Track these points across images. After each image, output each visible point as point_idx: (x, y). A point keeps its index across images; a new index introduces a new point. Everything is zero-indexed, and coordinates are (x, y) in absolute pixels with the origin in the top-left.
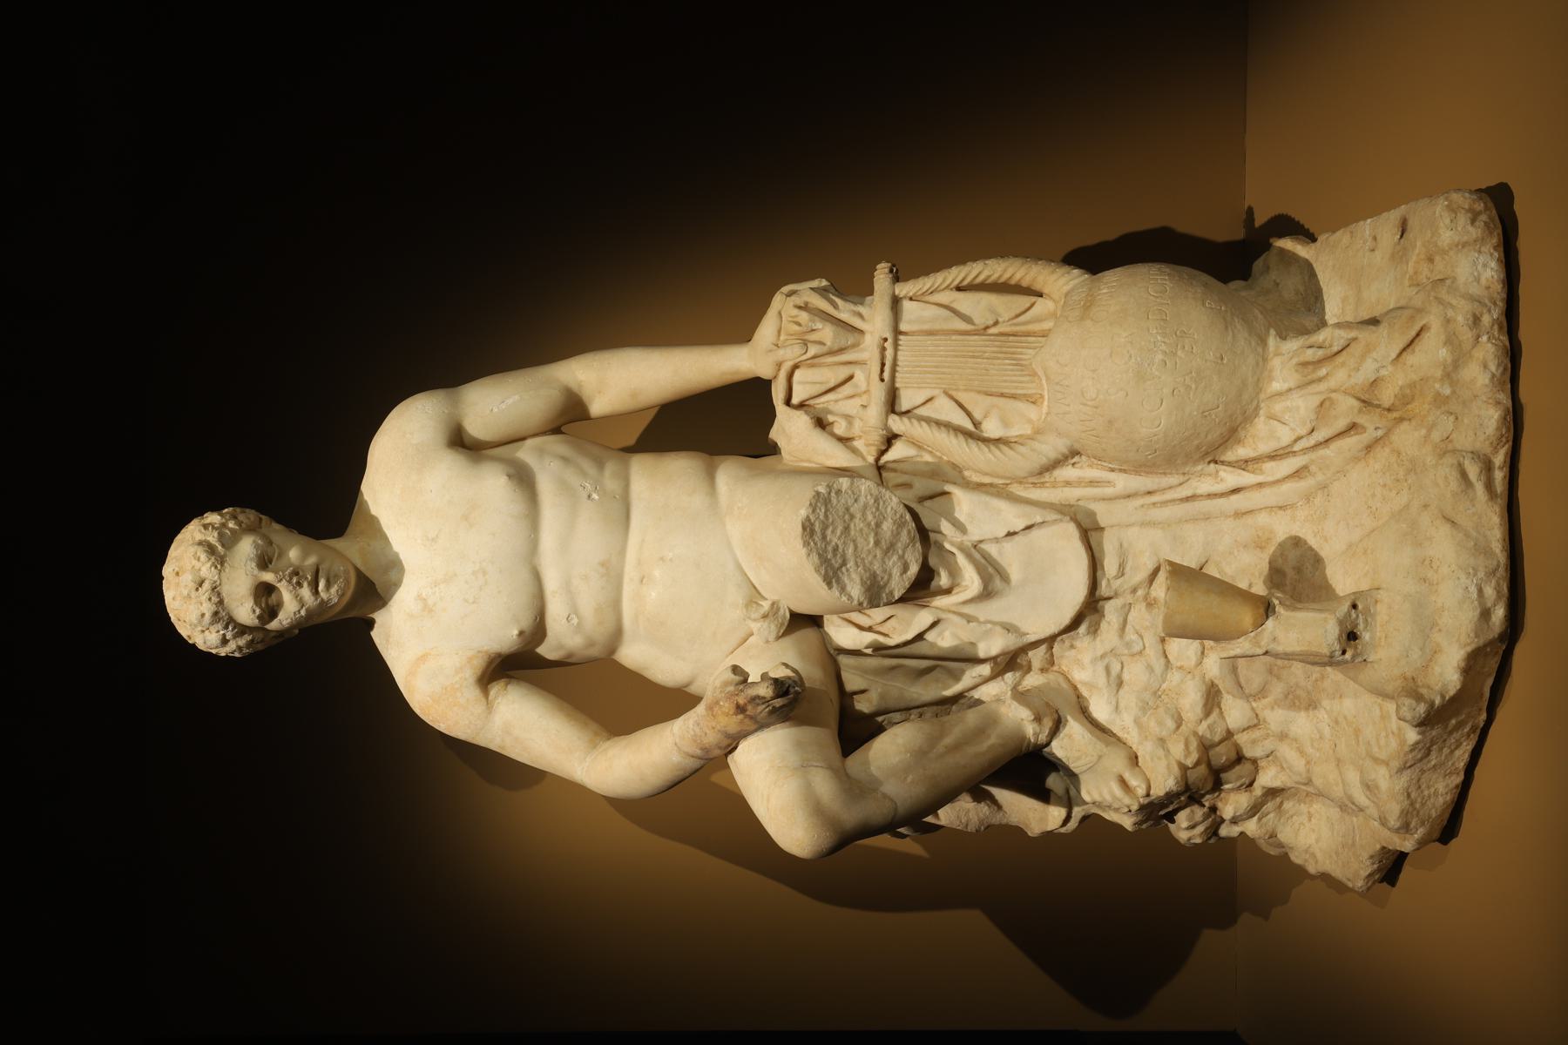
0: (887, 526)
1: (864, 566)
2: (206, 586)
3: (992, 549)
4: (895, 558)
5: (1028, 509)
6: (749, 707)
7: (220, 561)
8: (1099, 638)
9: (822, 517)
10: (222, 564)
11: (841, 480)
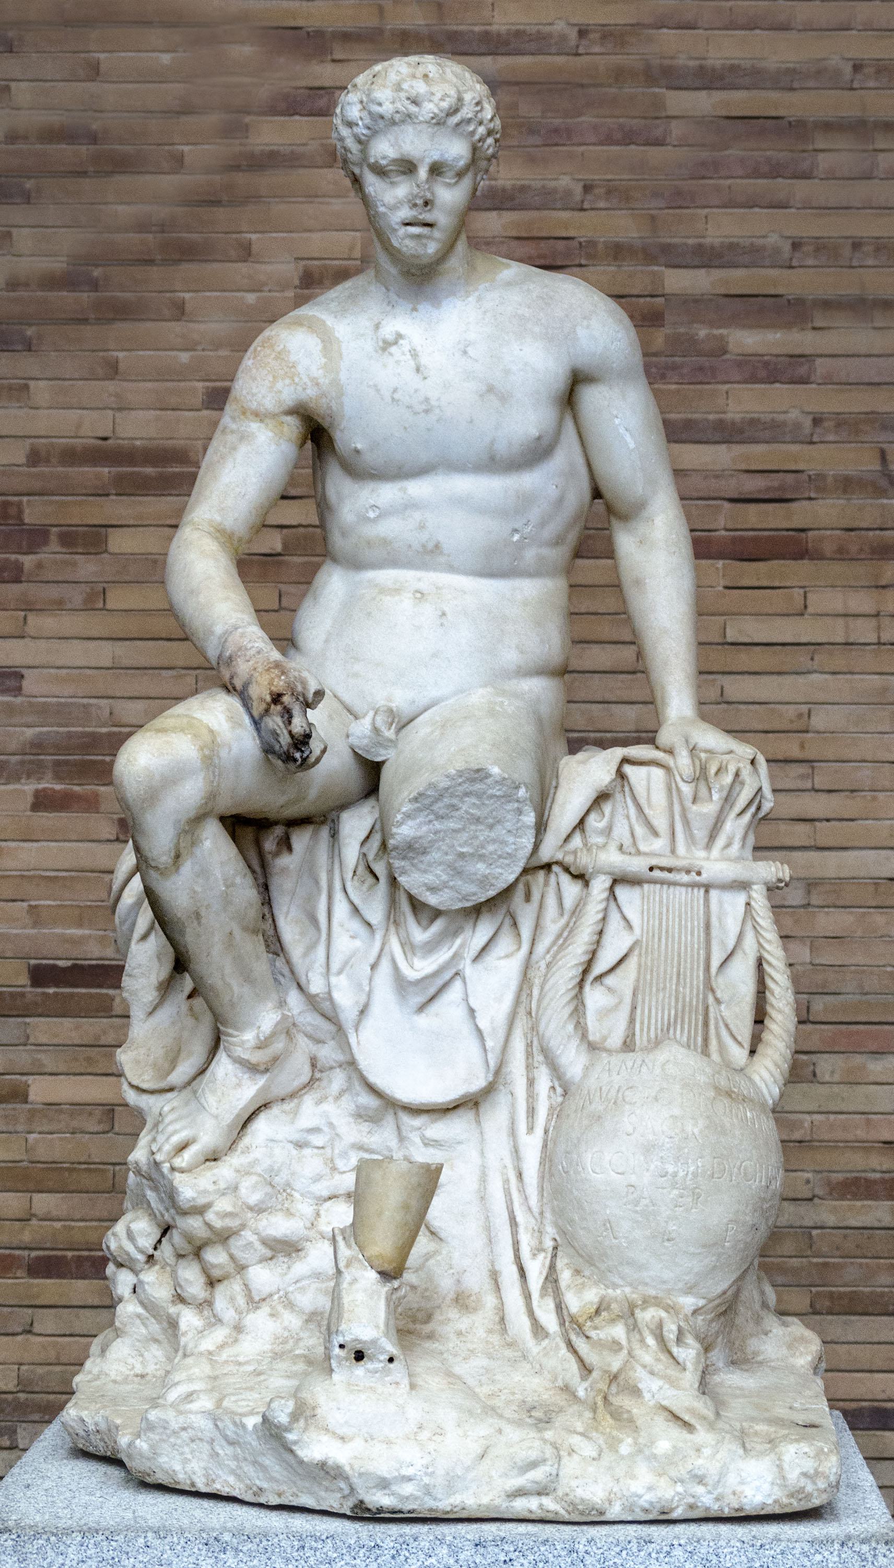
0: (481, 868)
1: (436, 841)
2: (413, 109)
3: (455, 992)
4: (444, 877)
5: (501, 1034)
6: (279, 708)
7: (438, 122)
8: (351, 1120)
9: (490, 792)
10: (438, 124)
11: (533, 814)
